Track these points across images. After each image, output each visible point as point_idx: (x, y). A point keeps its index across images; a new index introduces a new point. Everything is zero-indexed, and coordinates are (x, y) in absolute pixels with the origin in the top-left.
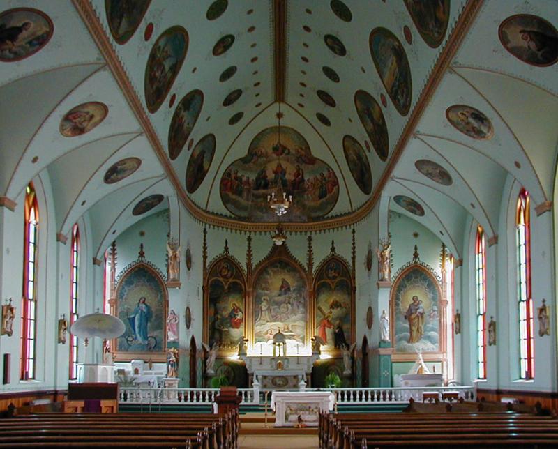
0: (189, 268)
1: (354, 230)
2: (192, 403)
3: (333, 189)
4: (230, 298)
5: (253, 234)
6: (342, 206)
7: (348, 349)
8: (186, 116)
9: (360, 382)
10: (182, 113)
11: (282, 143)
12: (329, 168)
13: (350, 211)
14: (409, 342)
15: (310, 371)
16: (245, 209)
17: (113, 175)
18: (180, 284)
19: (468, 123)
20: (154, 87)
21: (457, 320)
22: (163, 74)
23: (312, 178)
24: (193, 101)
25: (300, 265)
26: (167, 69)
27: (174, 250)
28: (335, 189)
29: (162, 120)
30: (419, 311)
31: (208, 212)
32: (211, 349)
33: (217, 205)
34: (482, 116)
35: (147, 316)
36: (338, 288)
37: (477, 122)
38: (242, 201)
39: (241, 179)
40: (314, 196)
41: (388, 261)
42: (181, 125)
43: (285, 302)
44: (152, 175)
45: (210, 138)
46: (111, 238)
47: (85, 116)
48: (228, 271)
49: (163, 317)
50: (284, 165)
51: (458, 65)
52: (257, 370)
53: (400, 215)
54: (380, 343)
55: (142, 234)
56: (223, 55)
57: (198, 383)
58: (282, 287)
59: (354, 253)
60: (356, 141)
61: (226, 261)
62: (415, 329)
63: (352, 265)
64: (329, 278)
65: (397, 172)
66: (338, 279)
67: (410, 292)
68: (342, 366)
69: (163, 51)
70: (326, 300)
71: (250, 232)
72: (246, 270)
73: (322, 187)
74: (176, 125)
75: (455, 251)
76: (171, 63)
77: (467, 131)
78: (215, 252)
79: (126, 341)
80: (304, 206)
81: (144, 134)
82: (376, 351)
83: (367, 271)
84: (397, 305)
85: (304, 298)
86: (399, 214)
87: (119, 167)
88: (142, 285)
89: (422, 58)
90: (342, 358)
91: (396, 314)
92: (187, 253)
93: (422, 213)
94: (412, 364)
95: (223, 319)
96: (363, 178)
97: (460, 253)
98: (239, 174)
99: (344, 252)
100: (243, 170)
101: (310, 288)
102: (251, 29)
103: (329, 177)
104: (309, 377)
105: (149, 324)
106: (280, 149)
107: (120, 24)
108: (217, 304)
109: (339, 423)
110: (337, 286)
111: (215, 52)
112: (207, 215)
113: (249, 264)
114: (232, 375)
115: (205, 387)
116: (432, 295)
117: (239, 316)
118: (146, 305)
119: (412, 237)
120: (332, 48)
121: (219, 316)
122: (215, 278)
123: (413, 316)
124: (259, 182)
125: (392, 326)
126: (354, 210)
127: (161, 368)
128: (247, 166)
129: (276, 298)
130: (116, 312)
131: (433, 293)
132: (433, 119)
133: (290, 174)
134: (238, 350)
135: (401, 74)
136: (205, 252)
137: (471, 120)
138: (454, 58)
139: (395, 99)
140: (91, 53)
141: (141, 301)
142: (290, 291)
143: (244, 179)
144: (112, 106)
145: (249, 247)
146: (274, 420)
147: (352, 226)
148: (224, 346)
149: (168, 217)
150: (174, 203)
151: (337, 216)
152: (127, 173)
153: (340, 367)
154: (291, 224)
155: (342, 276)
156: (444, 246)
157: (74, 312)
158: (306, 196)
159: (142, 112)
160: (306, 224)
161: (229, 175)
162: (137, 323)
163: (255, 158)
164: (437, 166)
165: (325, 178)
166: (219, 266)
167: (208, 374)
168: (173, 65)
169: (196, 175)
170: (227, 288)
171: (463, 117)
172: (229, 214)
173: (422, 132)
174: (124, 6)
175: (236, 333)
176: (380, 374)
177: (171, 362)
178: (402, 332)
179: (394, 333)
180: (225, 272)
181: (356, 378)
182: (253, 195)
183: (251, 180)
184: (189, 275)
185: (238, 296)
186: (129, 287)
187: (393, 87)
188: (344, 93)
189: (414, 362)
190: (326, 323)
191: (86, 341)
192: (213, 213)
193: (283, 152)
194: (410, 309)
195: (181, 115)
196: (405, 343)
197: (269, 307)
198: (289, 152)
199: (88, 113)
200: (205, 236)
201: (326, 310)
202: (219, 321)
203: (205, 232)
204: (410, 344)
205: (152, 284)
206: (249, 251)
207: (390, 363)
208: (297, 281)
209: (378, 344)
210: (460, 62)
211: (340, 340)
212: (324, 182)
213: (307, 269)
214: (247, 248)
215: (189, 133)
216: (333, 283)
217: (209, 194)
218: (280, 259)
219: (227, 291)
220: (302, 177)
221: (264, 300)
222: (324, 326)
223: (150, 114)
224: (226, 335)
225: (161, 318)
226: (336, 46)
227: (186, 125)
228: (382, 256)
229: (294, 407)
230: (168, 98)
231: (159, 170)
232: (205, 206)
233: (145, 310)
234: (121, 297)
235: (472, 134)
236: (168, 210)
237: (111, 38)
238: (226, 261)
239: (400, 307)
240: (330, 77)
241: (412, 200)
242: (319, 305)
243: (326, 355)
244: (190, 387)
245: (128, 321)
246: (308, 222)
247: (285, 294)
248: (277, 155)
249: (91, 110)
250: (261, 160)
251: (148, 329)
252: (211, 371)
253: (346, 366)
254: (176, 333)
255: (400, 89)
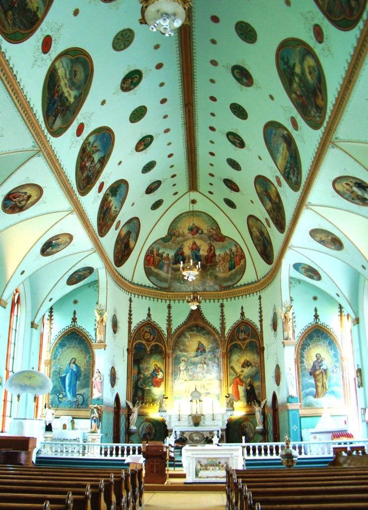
0: (115, 332)
1: (260, 296)
2: (106, 458)
3: (240, 262)
4: (152, 360)
5: (172, 302)
6: (249, 276)
7: (260, 405)
8: (114, 202)
9: (272, 438)
10: (110, 198)
11: (196, 225)
12: (236, 244)
13: (257, 280)
14: (315, 397)
15: (225, 427)
16: (165, 280)
17: (48, 248)
18: (105, 346)
19: (353, 192)
20: (85, 175)
21: (358, 374)
22: (93, 165)
23: (222, 253)
24: (119, 188)
25: (214, 329)
26: (96, 160)
27: (101, 315)
28: (242, 261)
29: (92, 202)
30: (322, 367)
31: (134, 284)
32: (134, 406)
33: (141, 277)
34: (364, 184)
35: (77, 375)
36: (248, 348)
37: (360, 190)
38: (163, 273)
39: (162, 256)
40: (224, 268)
41: (291, 321)
42: (109, 209)
43: (201, 363)
44: (82, 250)
45: (135, 221)
46: (47, 305)
47: (23, 196)
48: (151, 334)
49: (91, 376)
50: (198, 242)
51: (339, 140)
52: (176, 426)
53: (299, 281)
54: (288, 399)
55: (76, 302)
56: (144, 151)
57: (121, 439)
58: (198, 349)
59: (261, 316)
60: (257, 220)
61: (149, 326)
62: (320, 384)
63: (259, 327)
64: (240, 340)
65: (293, 241)
66: (248, 341)
67: (313, 350)
68: (254, 422)
69: (92, 145)
70: (238, 360)
71: (170, 300)
72: (166, 334)
73: (231, 261)
74: (105, 208)
75: (352, 311)
76: (100, 156)
77: (353, 199)
78: (139, 318)
79: (57, 399)
80: (216, 277)
81: (74, 212)
82: (285, 407)
83: (273, 331)
84: (302, 362)
85: (218, 359)
86: (299, 280)
87: (54, 242)
88: (74, 347)
89: (307, 140)
90: (255, 414)
91: (302, 371)
92: (113, 318)
93: (319, 278)
94: (319, 418)
95: (146, 379)
96: (266, 252)
97: (356, 312)
98: (161, 251)
99: (252, 316)
100: (164, 247)
101: (224, 349)
102: (167, 131)
103: (237, 252)
104: (224, 433)
105: (78, 382)
106: (195, 229)
107: (54, 121)
108: (141, 366)
109: (240, 480)
110: (247, 347)
111: (138, 149)
112: (133, 286)
113: (169, 329)
114: (154, 431)
115: (128, 443)
116: (333, 352)
117: (160, 375)
118: (76, 365)
119: (312, 300)
120: (233, 143)
121: (142, 376)
122: (140, 341)
123: (317, 372)
124: (177, 258)
125: (299, 384)
126: (259, 279)
127: (84, 425)
128: (167, 244)
129: (193, 359)
130: (50, 372)
131: (335, 351)
132: (321, 190)
133: (203, 250)
134: (158, 407)
135: (291, 157)
136: (130, 318)
137: (355, 189)
138: (335, 134)
139: (288, 180)
140: (27, 141)
141: (73, 361)
142: (205, 352)
143: (165, 255)
144: (46, 187)
145: (169, 314)
146: (184, 476)
147: (258, 292)
148: (146, 403)
149: (98, 287)
150: (102, 275)
151: (245, 285)
152: (62, 246)
153: (252, 423)
154: (206, 293)
155: (250, 338)
156: (341, 307)
157: (10, 370)
158: (217, 269)
159: (72, 194)
160: (218, 292)
161: (152, 252)
162: (67, 382)
163: (174, 237)
164: (328, 233)
165: (234, 253)
166: (143, 330)
167: (131, 430)
168: (101, 158)
169: (123, 252)
170: (149, 349)
171: (348, 187)
172: (151, 285)
173: (313, 203)
174: (59, 108)
175: (157, 391)
176: (289, 428)
177: (94, 418)
178: (308, 387)
179: (301, 388)
180: (147, 336)
181: (268, 433)
182: (172, 269)
183: (170, 256)
184: (115, 338)
185: (159, 357)
186: (62, 349)
187: (286, 169)
188: (245, 180)
189: (321, 416)
190: (239, 381)
191: (19, 396)
192: (138, 285)
193: (197, 232)
194: (314, 366)
195: (109, 200)
196: (311, 399)
197: (187, 367)
198: (202, 233)
199: (26, 193)
200: (130, 304)
201: (238, 368)
202: (141, 380)
203: (131, 301)
204: (316, 400)
205: (82, 346)
206: (169, 317)
207: (298, 418)
208: (212, 343)
209: (286, 399)
210: (340, 138)
211: (252, 397)
212: (232, 256)
213: (220, 332)
214: (168, 315)
215: (117, 215)
216: (243, 344)
217: (134, 268)
218: (196, 323)
219: (149, 353)
220: (214, 253)
221: (182, 360)
222: (237, 384)
223: (80, 196)
224: (149, 393)
225: (88, 377)
226: (236, 140)
227: (113, 209)
228: (285, 317)
229: (204, 462)
230: (97, 185)
231: (89, 244)
232: (131, 278)
233: (75, 370)
234: (55, 358)
235: (357, 201)
236: (96, 282)
237: (46, 131)
238: (149, 326)
239: (304, 364)
240: (233, 167)
241: (309, 266)
242: (232, 364)
243: (240, 410)
244: (114, 443)
245: (60, 380)
246: (220, 291)
247: (201, 355)
248: (192, 235)
249: (29, 191)
250: (179, 239)
251: (77, 387)
252: (133, 428)
253: (258, 422)
254: (101, 391)
255: (292, 170)
